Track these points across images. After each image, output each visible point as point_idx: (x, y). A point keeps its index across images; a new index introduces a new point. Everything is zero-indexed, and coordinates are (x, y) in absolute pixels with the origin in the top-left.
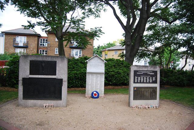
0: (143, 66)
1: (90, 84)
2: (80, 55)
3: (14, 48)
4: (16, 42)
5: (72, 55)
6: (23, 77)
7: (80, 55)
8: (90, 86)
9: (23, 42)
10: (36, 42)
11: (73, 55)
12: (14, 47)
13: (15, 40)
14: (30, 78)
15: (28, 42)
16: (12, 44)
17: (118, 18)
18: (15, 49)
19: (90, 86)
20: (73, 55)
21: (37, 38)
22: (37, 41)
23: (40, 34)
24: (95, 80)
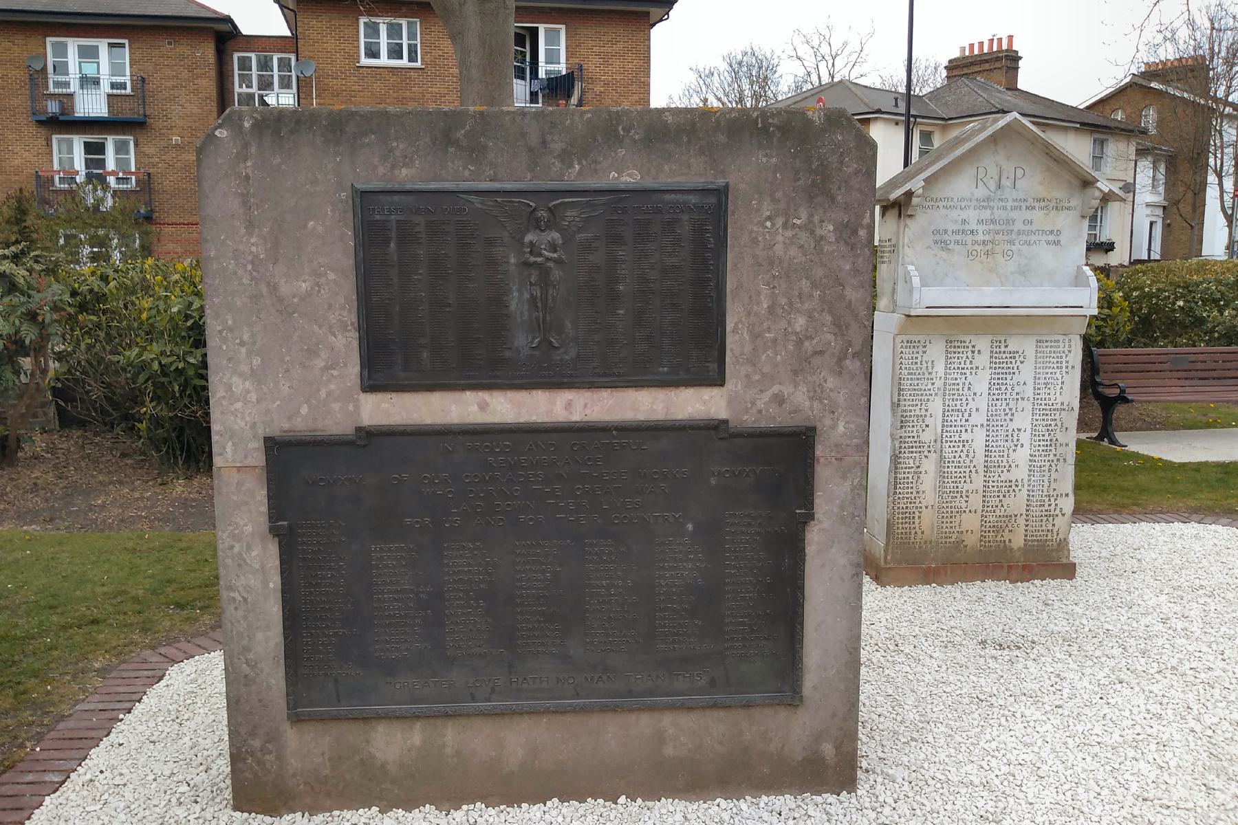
0: (812, 89)
1: (927, 436)
2: (113, 86)
3: (43, 131)
4: (52, 89)
5: (58, 84)
6: (281, 426)
7: (113, 86)
8: (929, 465)
9: (105, 87)
10: (208, 85)
11: (67, 84)
12: (40, 123)
13: (38, 77)
14: (370, 437)
15: (141, 82)
16: (20, 100)
17: (1101, 216)
18: (49, 144)
19: (929, 465)
20: (67, 84)
21: (207, 52)
22: (213, 73)
23: (228, 20)
24: (982, 403)
